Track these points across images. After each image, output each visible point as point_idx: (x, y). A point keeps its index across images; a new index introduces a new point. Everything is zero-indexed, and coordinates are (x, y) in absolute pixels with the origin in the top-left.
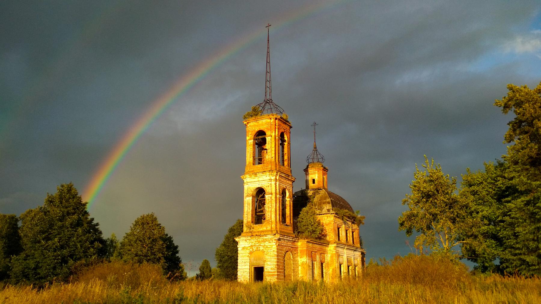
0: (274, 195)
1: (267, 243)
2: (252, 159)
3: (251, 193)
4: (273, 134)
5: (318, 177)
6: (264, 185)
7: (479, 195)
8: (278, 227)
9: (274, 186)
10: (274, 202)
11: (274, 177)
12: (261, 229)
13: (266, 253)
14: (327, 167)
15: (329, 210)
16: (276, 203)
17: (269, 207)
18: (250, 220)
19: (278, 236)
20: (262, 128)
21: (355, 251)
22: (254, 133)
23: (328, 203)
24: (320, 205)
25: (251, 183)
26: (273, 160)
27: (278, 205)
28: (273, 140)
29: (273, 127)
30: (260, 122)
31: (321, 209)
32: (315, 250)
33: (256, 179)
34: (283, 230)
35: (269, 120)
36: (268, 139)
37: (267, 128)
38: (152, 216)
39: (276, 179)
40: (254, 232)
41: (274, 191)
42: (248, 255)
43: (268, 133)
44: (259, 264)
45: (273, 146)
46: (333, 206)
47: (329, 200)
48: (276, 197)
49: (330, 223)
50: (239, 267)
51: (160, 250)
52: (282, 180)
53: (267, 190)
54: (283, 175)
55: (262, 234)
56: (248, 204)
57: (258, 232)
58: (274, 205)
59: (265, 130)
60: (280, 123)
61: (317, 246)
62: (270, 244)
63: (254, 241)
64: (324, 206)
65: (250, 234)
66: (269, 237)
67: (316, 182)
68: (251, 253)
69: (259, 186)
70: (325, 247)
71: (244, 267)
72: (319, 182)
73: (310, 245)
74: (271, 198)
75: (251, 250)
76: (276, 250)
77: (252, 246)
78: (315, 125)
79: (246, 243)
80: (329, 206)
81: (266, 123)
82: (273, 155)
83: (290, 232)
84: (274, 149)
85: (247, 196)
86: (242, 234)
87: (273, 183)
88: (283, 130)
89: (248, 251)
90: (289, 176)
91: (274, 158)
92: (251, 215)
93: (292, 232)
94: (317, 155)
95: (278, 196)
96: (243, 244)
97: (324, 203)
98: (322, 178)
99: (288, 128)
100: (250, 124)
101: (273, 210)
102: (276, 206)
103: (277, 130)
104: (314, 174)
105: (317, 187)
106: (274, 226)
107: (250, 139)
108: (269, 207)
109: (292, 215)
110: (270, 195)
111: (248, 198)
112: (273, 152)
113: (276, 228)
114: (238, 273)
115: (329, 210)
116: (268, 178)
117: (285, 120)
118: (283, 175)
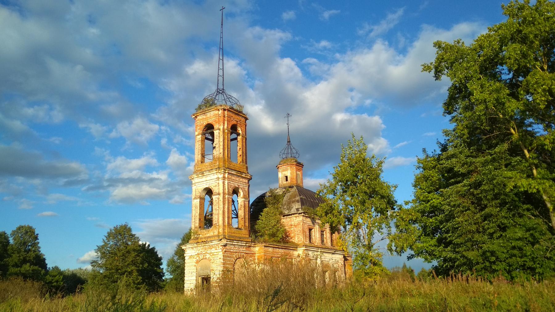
0: (222, 195)
1: (213, 251)
2: (200, 156)
3: (199, 195)
4: (221, 127)
5: (291, 174)
6: (212, 185)
7: (431, 180)
8: (226, 231)
9: (222, 185)
10: (221, 203)
11: (222, 175)
12: (208, 235)
13: (212, 261)
14: (302, 162)
15: (297, 210)
16: (224, 204)
17: (216, 209)
18: (197, 225)
19: (224, 242)
20: (210, 121)
21: (333, 254)
22: (202, 127)
23: (298, 201)
24: (289, 205)
25: (199, 184)
26: (221, 156)
27: (226, 207)
28: (221, 133)
29: (221, 119)
30: (208, 115)
31: (289, 209)
32: (276, 256)
33: (204, 179)
34: (233, 234)
35: (217, 112)
36: (216, 133)
37: (215, 121)
38: (125, 226)
39: (224, 177)
40: (201, 238)
41: (221, 191)
42: (195, 264)
43: (216, 126)
44: (204, 273)
45: (221, 140)
46: (302, 204)
47: (298, 198)
48: (224, 198)
49: (299, 224)
50: (186, 278)
51: (134, 263)
52: (233, 178)
53: (215, 190)
54: (233, 172)
55: (209, 240)
56: (196, 207)
57: (205, 238)
58: (222, 206)
59: (213, 123)
60: (230, 114)
61: (280, 250)
62: (216, 251)
63: (200, 249)
64: (293, 205)
65: (196, 241)
66: (215, 242)
67: (289, 179)
68: (197, 262)
69: (207, 186)
70: (292, 251)
71: (190, 278)
72: (292, 179)
73: (270, 249)
74: (219, 199)
75: (198, 258)
76: (222, 258)
77: (198, 254)
78: (288, 117)
79: (193, 251)
80: (297, 205)
81: (212, 116)
82: (222, 151)
83: (244, 236)
84: (222, 144)
85: (195, 198)
86: (190, 242)
87: (221, 182)
88: (235, 122)
89: (195, 260)
90: (242, 173)
91: (222, 154)
92: (198, 219)
93: (248, 236)
94: (291, 148)
95: (227, 196)
96: (190, 251)
97: (293, 202)
98: (295, 174)
99: (243, 119)
100: (198, 118)
101: (221, 212)
102: (224, 207)
103: (226, 122)
104: (287, 170)
105: (289, 185)
106: (221, 230)
107: (198, 135)
108: (216, 209)
109: (247, 216)
110: (218, 196)
111: (195, 201)
112: (222, 147)
113: (224, 232)
114: (185, 285)
115: (297, 210)
116: (216, 176)
117: (237, 111)
118: (233, 172)
